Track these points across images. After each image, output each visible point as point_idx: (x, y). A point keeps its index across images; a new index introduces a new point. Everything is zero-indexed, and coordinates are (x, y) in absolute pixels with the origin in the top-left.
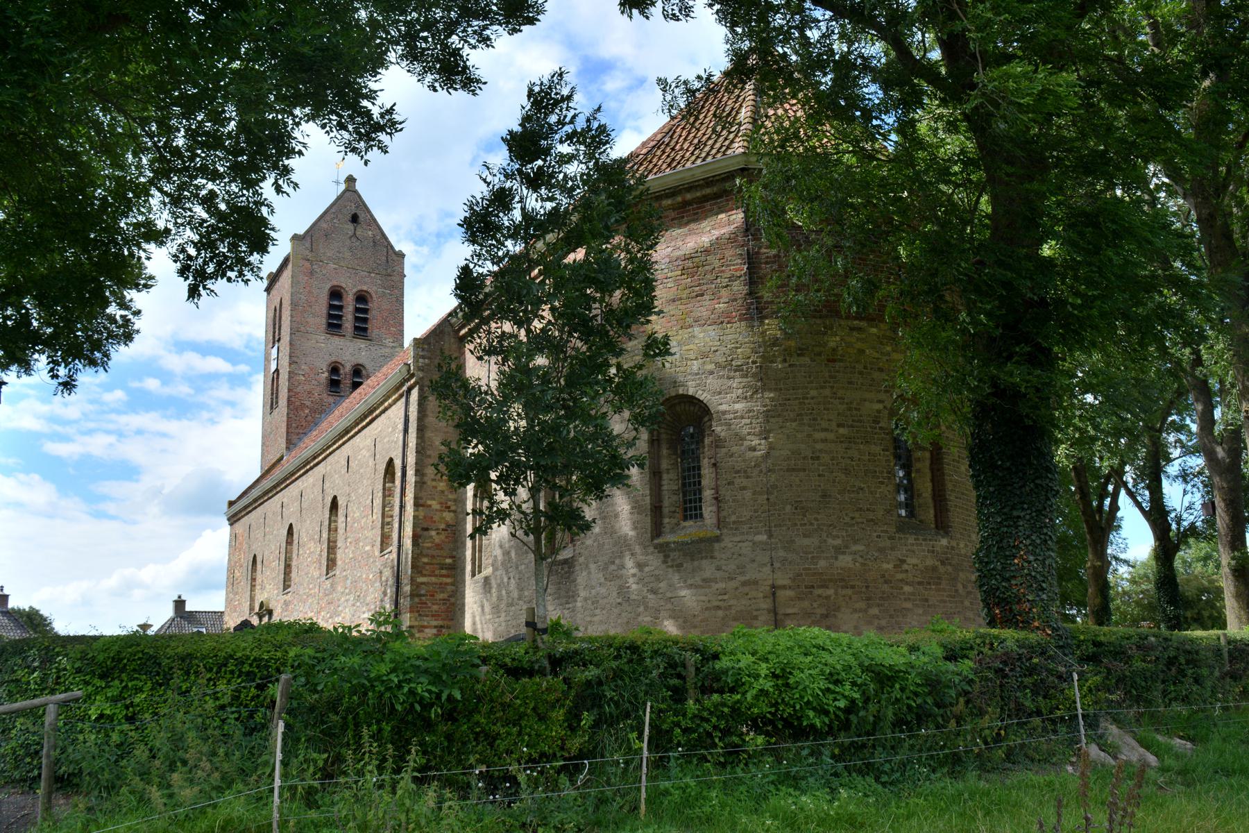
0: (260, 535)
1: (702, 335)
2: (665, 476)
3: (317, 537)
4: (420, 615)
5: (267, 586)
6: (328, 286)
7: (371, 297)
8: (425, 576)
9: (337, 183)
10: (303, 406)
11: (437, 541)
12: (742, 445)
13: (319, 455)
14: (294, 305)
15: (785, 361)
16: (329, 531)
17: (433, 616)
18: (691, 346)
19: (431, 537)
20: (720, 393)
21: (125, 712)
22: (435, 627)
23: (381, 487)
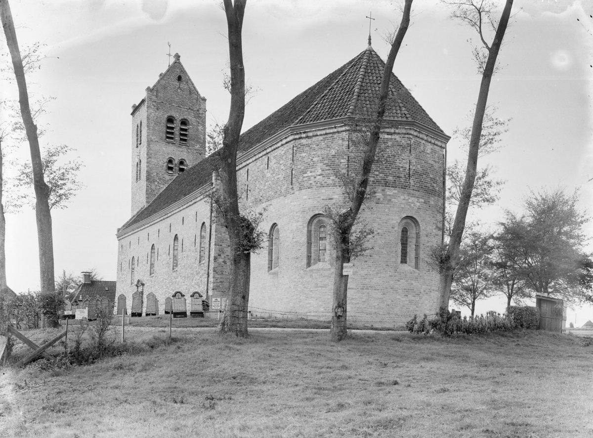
2: (313, 244)
6: (166, 116)
23: (199, 234)
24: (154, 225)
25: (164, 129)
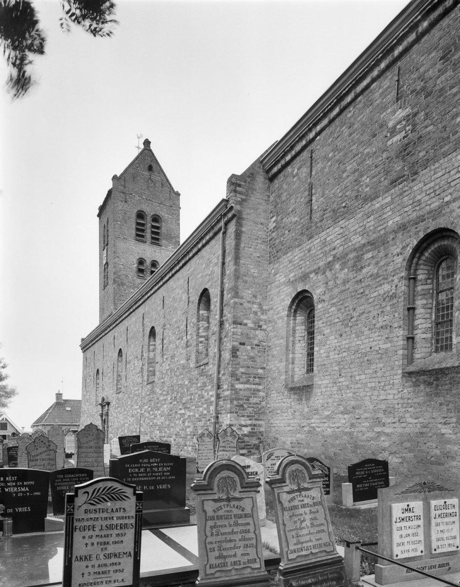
0: (101, 357)
3: (140, 357)
6: (136, 211)
9: (139, 148)
11: (252, 354)
17: (248, 416)
21: (309, 180)
22: (251, 425)
24: (120, 324)
25: (134, 226)
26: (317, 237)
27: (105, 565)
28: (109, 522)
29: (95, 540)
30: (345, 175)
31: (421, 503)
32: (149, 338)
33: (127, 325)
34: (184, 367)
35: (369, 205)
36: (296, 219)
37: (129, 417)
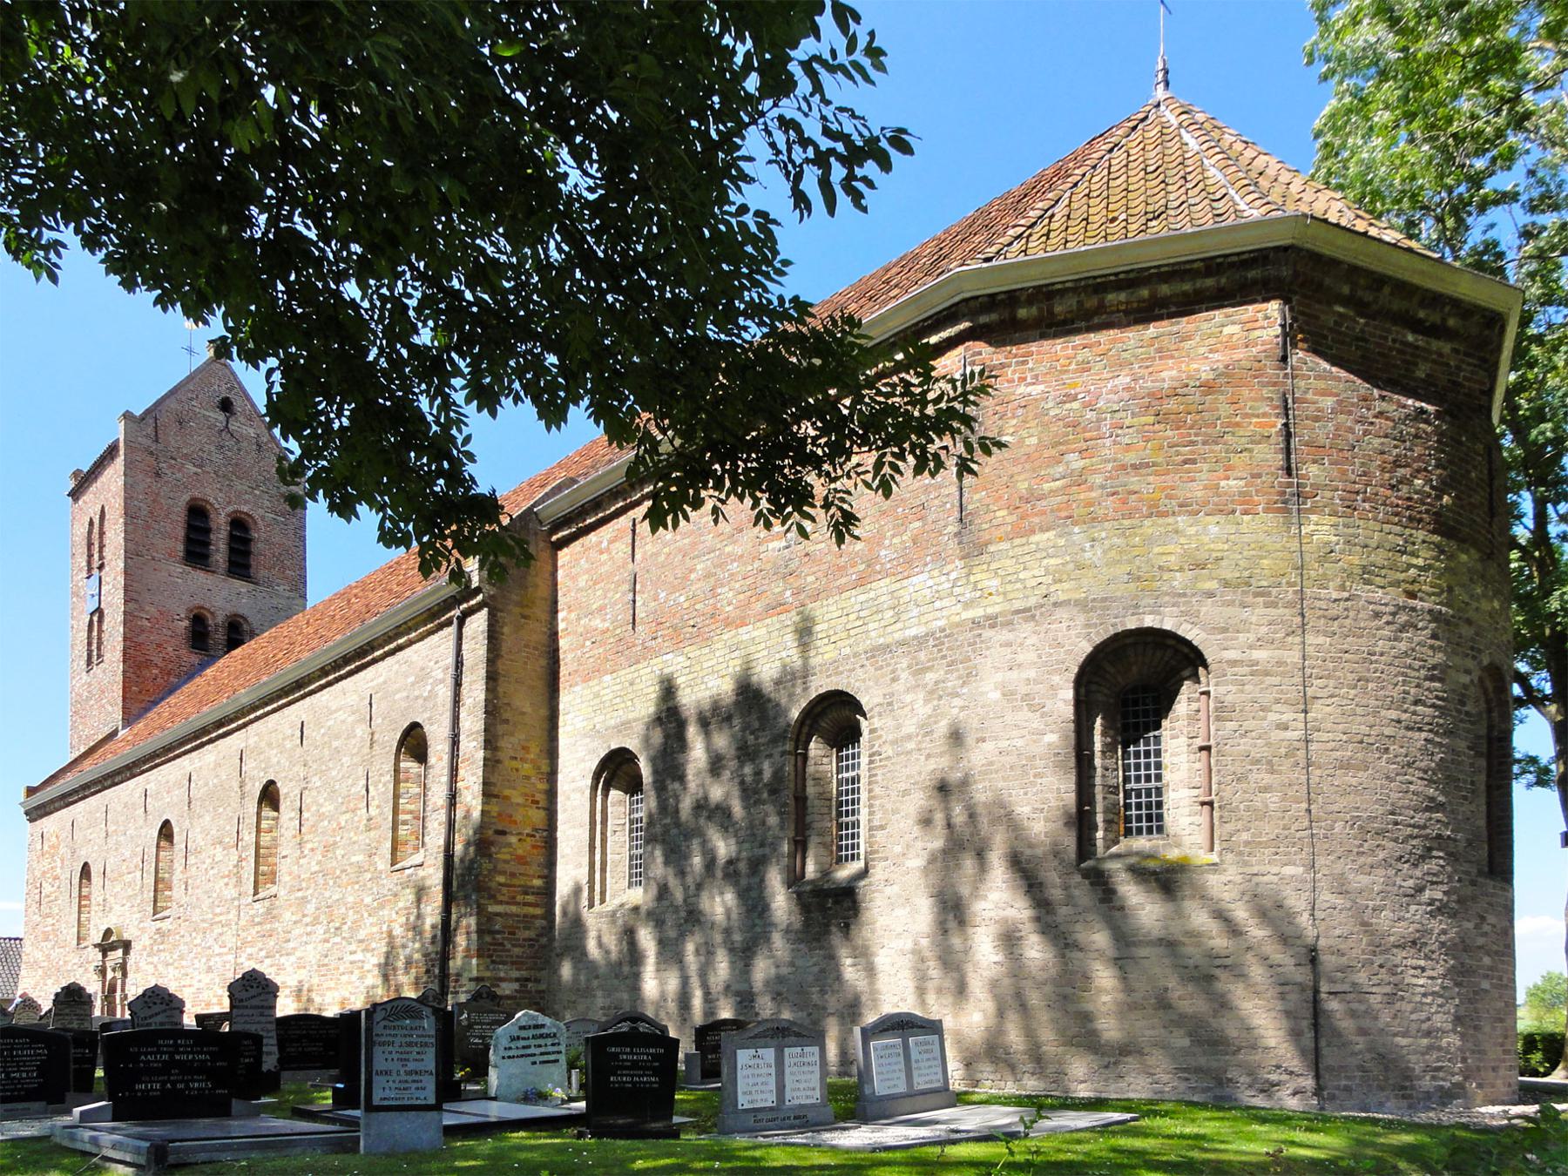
1: (1192, 531)
4: (493, 962)
5: (117, 907)
6: (186, 497)
7: (256, 523)
8: (501, 903)
10: (148, 664)
11: (520, 852)
12: (1264, 719)
13: (232, 721)
14: (130, 514)
15: (1343, 588)
16: (258, 830)
17: (513, 963)
18: (1170, 548)
19: (509, 845)
20: (1225, 630)
22: (517, 980)
26: (646, 664)
27: (406, 1081)
28: (408, 1039)
29: (395, 1056)
30: (693, 576)
31: (772, 1050)
32: (260, 802)
33: (189, 769)
34: (361, 870)
35: (733, 633)
36: (607, 625)
37: (196, 973)
